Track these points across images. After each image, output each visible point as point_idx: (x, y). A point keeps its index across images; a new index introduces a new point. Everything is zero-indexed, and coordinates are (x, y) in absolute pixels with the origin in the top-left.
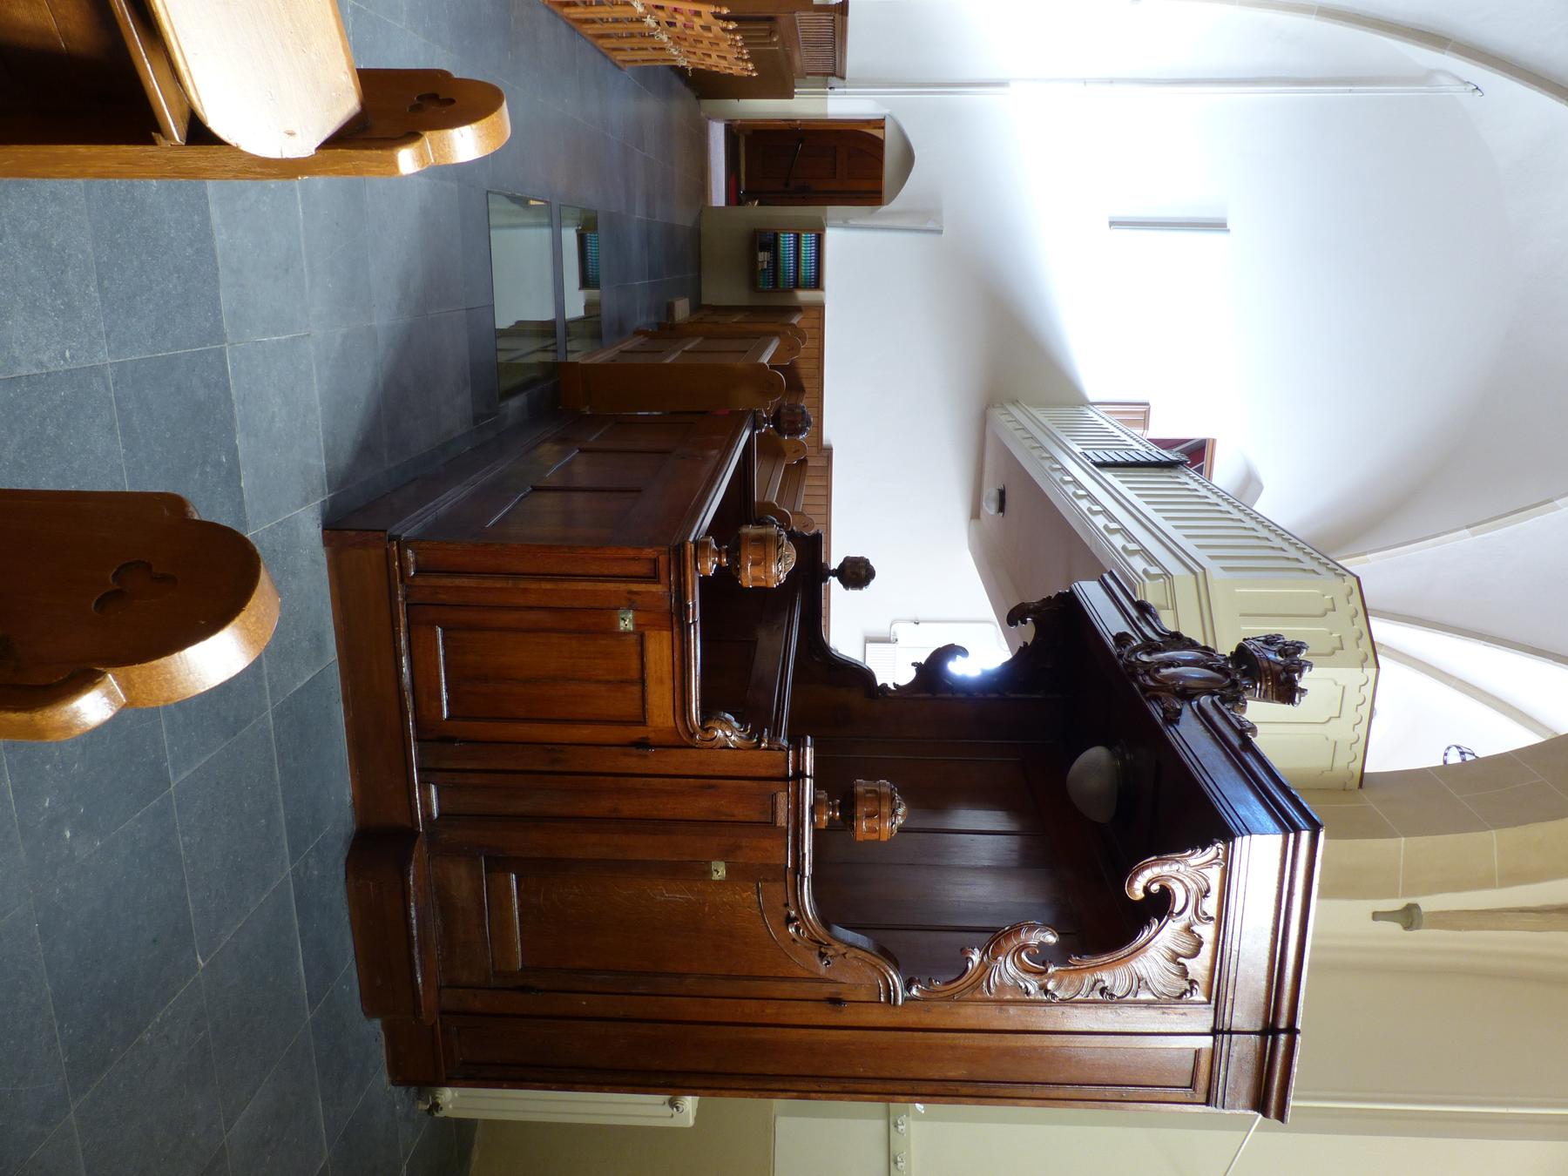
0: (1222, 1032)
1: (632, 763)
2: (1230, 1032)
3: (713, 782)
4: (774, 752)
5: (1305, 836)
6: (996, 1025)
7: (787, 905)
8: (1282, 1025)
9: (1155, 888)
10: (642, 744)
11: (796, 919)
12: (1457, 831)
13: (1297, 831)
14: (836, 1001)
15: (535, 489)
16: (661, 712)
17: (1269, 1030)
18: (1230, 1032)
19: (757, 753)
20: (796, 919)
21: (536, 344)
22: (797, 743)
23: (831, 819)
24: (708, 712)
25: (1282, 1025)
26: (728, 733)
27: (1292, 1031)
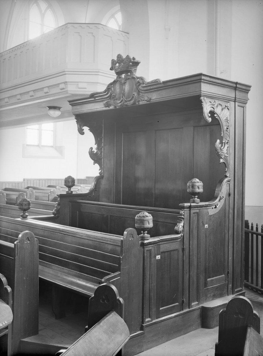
0: (235, 100)
1: (187, 251)
2: (235, 98)
3: (191, 230)
4: (185, 213)
5: (203, 77)
6: (233, 167)
7: (213, 208)
8: (235, 85)
9: (210, 115)
10: (183, 249)
11: (215, 206)
12: (206, 307)
13: (201, 79)
14: (229, 195)
15: (65, 34)
16: (175, 246)
17: (235, 89)
18: (235, 98)
19: (185, 215)
20: (215, 206)
21: (28, 128)
22: (183, 208)
23: (198, 198)
24: (177, 233)
25: (235, 85)
26: (180, 226)
27: (236, 83)
